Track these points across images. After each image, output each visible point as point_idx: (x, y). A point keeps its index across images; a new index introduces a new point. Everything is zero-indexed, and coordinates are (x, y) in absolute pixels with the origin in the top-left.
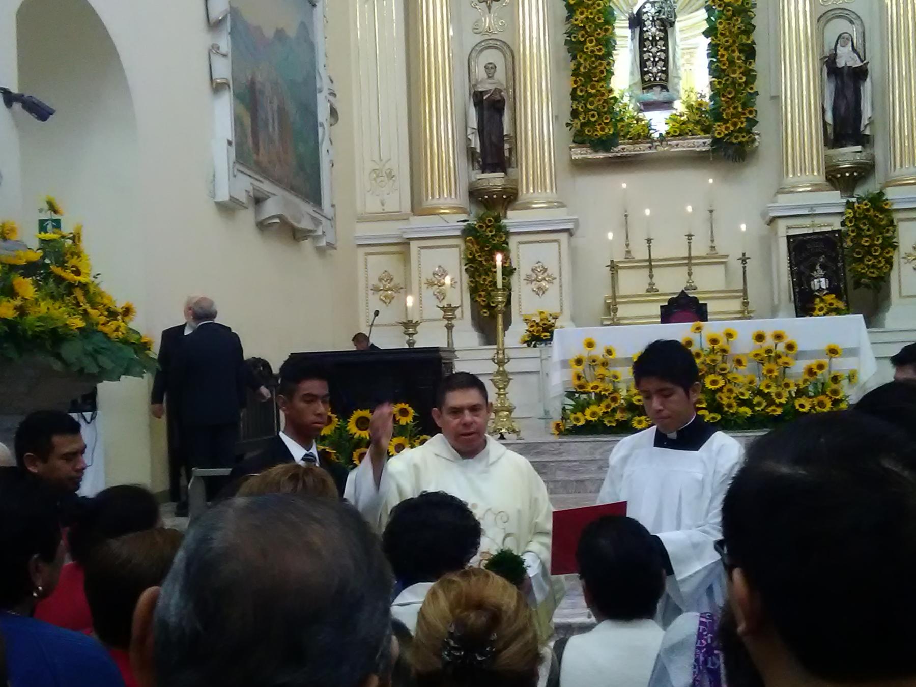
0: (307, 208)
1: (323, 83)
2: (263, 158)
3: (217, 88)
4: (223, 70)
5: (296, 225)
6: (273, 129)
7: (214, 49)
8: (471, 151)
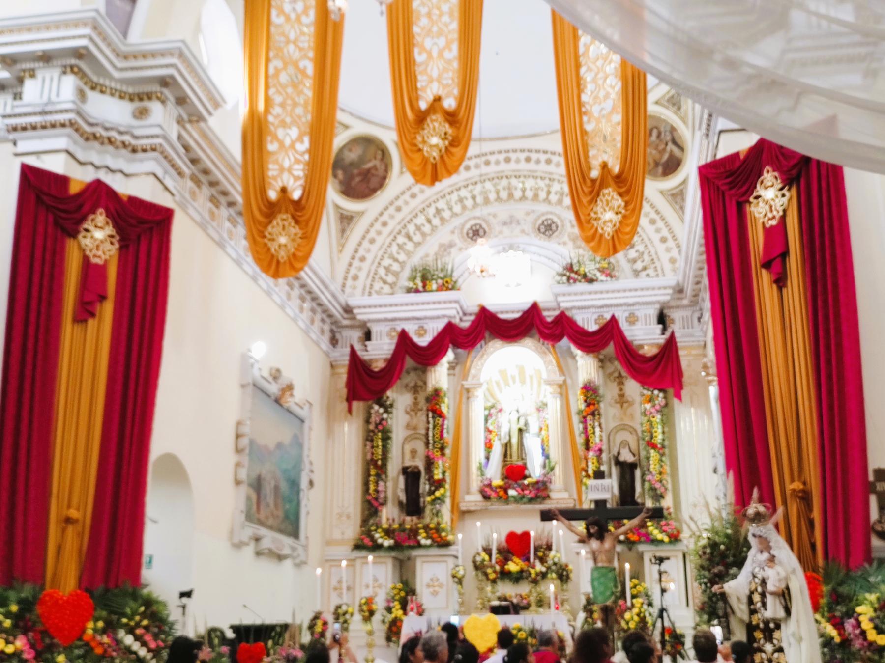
0: (287, 541)
1: (307, 467)
2: (262, 516)
3: (238, 483)
4: (243, 474)
5: (280, 552)
6: (270, 500)
7: (238, 465)
8: (400, 503)
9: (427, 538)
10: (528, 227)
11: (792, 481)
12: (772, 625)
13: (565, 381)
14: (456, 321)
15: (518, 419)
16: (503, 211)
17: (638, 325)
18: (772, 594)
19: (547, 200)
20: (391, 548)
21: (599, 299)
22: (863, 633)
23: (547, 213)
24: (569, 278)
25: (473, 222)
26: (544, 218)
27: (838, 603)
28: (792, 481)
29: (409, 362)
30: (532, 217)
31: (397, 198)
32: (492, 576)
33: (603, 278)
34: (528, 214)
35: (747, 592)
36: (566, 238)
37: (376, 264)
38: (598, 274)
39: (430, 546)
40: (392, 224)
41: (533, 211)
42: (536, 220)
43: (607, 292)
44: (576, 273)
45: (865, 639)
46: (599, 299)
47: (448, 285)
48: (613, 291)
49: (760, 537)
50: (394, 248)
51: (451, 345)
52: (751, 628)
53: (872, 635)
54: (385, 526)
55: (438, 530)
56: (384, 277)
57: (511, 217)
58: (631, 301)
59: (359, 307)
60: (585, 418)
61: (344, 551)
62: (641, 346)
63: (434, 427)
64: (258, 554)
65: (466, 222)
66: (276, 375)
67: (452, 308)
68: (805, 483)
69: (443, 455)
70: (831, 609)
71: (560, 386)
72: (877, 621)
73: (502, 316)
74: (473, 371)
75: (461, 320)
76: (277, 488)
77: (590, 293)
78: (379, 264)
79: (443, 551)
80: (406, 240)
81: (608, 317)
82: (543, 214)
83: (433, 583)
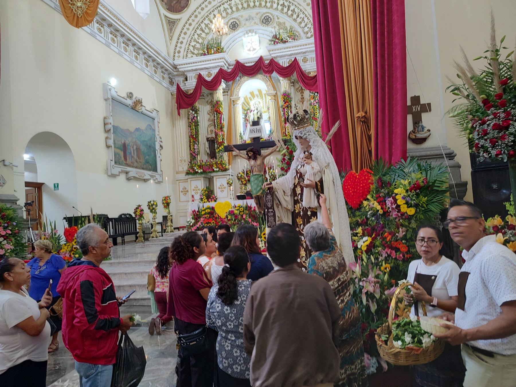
1: (158, 139)
3: (108, 147)
4: (111, 142)
7: (107, 138)
8: (208, 153)
9: (217, 168)
10: (257, 21)
11: (358, 111)
12: (309, 213)
13: (276, 93)
14: (225, 68)
15: (257, 113)
16: (245, 14)
17: (308, 62)
18: (307, 186)
19: (265, 6)
20: (201, 173)
21: (289, 51)
22: (398, 207)
23: (266, 13)
24: (275, 42)
25: (232, 21)
26: (265, 16)
27: (383, 188)
28: (358, 111)
29: (204, 90)
30: (259, 15)
31: (195, 11)
32: (244, 182)
33: (291, 40)
34: (257, 14)
35: (292, 186)
36: (275, 25)
37: (188, 44)
38: (288, 39)
39: (218, 171)
40: (194, 24)
41: (260, 12)
42: (261, 17)
43: (293, 47)
44: (278, 39)
45: (399, 211)
46: (289, 51)
47: (219, 50)
48: (295, 47)
49: (301, 138)
50: (196, 36)
51: (223, 80)
52: (295, 215)
53: (404, 208)
54: (199, 164)
55: (221, 164)
56: (193, 51)
57: (249, 16)
58: (304, 50)
59: (180, 65)
60: (284, 109)
61: (183, 176)
62: (310, 73)
63: (217, 119)
64: (128, 179)
65: (229, 21)
66: (130, 95)
67: (221, 62)
68: (366, 113)
69: (222, 131)
70: (377, 192)
71: (275, 96)
72: (408, 199)
73: (246, 65)
74: (235, 93)
75: (228, 68)
76: (138, 149)
77: (285, 48)
78: (189, 44)
79: (224, 173)
80: (201, 32)
81: (293, 59)
82: (264, 14)
83: (221, 188)
